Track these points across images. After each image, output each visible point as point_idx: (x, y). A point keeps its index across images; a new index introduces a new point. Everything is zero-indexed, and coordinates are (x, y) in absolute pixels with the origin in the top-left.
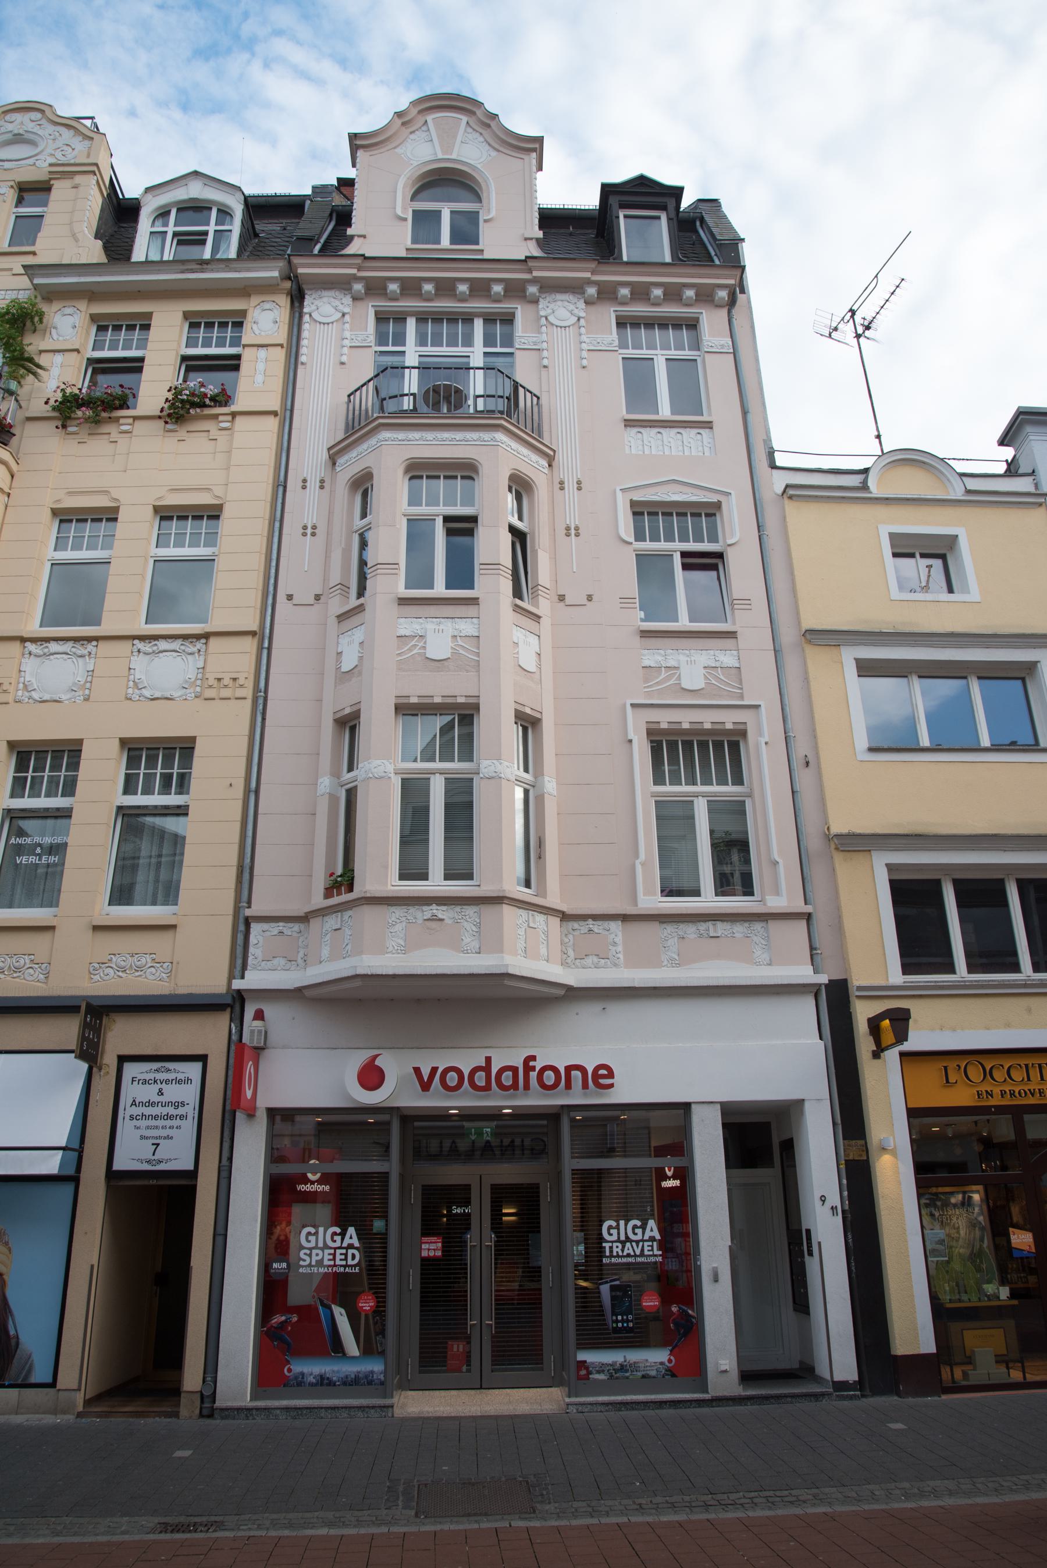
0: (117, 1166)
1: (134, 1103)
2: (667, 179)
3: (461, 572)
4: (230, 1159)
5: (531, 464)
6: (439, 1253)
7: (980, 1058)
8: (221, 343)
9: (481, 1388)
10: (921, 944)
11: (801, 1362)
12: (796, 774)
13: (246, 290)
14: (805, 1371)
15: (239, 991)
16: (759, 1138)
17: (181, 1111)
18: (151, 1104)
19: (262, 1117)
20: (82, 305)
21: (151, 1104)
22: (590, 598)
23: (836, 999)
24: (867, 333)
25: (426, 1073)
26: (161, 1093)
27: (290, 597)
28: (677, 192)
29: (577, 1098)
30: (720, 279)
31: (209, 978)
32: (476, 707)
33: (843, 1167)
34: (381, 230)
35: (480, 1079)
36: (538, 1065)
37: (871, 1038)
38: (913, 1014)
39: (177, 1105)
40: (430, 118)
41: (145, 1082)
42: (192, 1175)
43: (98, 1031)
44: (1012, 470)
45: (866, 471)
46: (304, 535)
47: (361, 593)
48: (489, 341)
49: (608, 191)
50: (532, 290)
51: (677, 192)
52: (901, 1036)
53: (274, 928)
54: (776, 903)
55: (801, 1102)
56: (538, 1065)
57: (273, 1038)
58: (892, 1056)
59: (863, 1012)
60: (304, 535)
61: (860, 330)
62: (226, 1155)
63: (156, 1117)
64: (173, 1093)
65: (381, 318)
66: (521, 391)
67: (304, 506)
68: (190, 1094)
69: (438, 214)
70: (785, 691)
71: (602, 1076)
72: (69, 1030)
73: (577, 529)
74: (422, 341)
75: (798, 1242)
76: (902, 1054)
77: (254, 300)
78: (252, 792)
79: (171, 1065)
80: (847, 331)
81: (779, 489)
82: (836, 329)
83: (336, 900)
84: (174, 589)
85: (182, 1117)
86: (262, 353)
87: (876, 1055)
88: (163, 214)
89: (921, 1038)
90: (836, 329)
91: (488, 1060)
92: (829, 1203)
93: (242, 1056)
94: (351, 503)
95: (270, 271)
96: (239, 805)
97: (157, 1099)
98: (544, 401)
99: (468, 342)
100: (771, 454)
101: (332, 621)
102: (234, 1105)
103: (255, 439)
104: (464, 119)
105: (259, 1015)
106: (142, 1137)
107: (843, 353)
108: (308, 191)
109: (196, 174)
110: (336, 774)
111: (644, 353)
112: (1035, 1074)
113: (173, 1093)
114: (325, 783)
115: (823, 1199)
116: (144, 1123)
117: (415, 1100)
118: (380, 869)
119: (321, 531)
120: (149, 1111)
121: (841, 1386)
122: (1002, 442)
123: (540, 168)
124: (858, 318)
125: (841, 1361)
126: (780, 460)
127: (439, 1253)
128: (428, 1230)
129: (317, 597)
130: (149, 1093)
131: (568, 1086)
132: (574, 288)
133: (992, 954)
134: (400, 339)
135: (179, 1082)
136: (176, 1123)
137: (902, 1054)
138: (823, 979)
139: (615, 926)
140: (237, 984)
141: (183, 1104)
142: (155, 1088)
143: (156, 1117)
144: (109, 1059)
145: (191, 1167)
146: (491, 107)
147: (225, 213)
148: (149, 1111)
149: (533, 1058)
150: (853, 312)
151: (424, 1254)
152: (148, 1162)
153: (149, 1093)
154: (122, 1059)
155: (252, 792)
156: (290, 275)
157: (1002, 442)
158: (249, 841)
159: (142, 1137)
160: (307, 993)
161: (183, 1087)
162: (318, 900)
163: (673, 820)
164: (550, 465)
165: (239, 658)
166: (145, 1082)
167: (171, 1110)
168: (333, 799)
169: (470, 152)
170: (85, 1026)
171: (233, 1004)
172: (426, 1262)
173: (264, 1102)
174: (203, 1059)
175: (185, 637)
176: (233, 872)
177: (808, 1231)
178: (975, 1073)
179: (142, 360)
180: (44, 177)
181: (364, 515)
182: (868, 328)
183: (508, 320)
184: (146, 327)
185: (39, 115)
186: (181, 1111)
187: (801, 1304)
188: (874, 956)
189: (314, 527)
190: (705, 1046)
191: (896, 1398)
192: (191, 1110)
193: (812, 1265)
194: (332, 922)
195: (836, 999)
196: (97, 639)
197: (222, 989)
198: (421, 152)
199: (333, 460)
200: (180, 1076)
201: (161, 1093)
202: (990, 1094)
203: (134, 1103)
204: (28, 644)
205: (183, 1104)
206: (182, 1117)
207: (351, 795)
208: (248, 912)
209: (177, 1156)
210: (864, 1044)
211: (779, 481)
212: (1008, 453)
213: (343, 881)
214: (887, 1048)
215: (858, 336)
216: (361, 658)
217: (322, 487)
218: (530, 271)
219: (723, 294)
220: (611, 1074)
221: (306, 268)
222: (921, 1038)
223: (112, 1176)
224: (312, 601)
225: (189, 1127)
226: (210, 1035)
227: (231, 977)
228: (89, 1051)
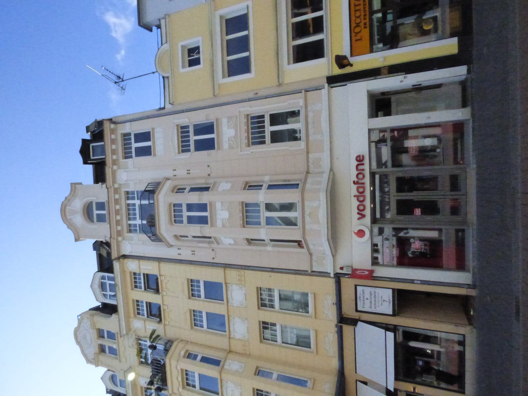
0: (391, 313)
1: (371, 307)
2: (79, 145)
3: (203, 207)
4: (389, 278)
5: (167, 186)
6: (420, 209)
7: (352, 28)
8: (140, 279)
9: (466, 195)
10: (313, 52)
11: (459, 84)
12: (353, 44)
13: (123, 272)
14: (463, 84)
15: (334, 275)
16: (381, 105)
17: (373, 293)
18: (371, 302)
19: (375, 268)
20: (131, 320)
21: (371, 302)
22: (208, 166)
23: (332, 80)
24: (122, 78)
25: (359, 216)
26: (367, 299)
27: (213, 258)
28: (84, 141)
29: (366, 167)
30: (107, 127)
31: (331, 283)
32: (243, 202)
33: (390, 75)
34: (102, 231)
35: (361, 199)
36: (356, 180)
37: (346, 68)
38: (337, 54)
39: (371, 294)
40: (68, 217)
41: (364, 304)
42: (394, 290)
43: (348, 319)
44: (159, 27)
45: (163, 77)
46: (194, 254)
47: (210, 238)
48: (133, 198)
49: (85, 162)
50: (116, 186)
51: (84, 141)
52: (345, 57)
53: (314, 264)
54: (301, 102)
55: (368, 91)
56: (356, 180)
57: (349, 264)
58: (352, 60)
59: (337, 71)
60: (194, 254)
61: (121, 80)
62: (387, 279)
63: (375, 301)
64: (367, 296)
65: (130, 231)
66: (147, 189)
67: (186, 254)
68: (367, 290)
69: (98, 215)
70: (239, 98)
71: (360, 160)
72: (347, 329)
73: (187, 171)
74: (135, 219)
75: (418, 89)
76: (352, 55)
77: (126, 269)
78: (273, 270)
79: (358, 296)
80: (122, 84)
81: (170, 106)
82: (122, 88)
83: (305, 246)
84: (214, 291)
85: (375, 293)
86: (141, 267)
87: (351, 65)
88: (105, 295)
89: (346, 51)
90: (122, 88)
91: (355, 196)
92: (403, 80)
93: (355, 274)
94: (184, 240)
95: (116, 265)
96: (276, 274)
97: (369, 301)
98: (150, 182)
99: (134, 205)
100: (161, 109)
101: (220, 246)
102: (370, 276)
103: (167, 269)
104: (68, 207)
105: (342, 268)
106: (382, 305)
107: (128, 84)
108: (95, 252)
109: (91, 286)
110: (266, 245)
111: (133, 150)
112: (357, 8)
113: (367, 296)
114: (269, 248)
115: (402, 81)
116: (377, 305)
117: (368, 219)
118: (293, 233)
119: (193, 249)
120: (373, 302)
121: (469, 71)
122: (151, 30)
123: (81, 184)
124: (117, 81)
125: (461, 71)
126: (162, 106)
127: (420, 209)
128: (411, 213)
129: (213, 250)
130: (367, 302)
131: (363, 170)
132: (114, 173)
133: (318, 25)
134: (135, 225)
135: (363, 293)
136: (377, 295)
137: (352, 55)
138: (326, 85)
139: (311, 156)
140: (332, 275)
141: (371, 292)
142: (366, 301)
143: (375, 301)
144: (356, 315)
145: (391, 290)
146: (63, 199)
147: (103, 278)
148: (373, 302)
149: (354, 182)
150: (116, 83)
151: (420, 214)
152: (389, 303)
153: (367, 302)
154: (357, 310)
155: (273, 270)
156: (118, 258)
157: (151, 30)
158: (287, 271)
159: (382, 305)
160: (334, 253)
161: (365, 292)
162: (304, 250)
163: (276, 137)
164: (169, 179)
165: (232, 274)
166: (364, 304)
167: (373, 296)
168: (274, 246)
169: (78, 204)
170: (346, 323)
171: (338, 277)
172: (423, 213)
173: (370, 267)
174: (356, 286)
175: (227, 290)
176: (297, 276)
177: (413, 86)
178: (357, 30)
179: (146, 303)
180: (95, 331)
181: (187, 237)
182: (120, 78)
183: (127, 193)
184: (137, 301)
185: (78, 332)
186: (373, 293)
187: (439, 86)
188: (320, 68)
189: (192, 251)
190: (345, 127)
191: (473, 52)
192: (373, 290)
193: (424, 84)
194: (311, 247)
195: (332, 80)
196: (228, 316)
197: (334, 280)
198: (79, 220)
199: (172, 246)
200: (362, 293)
201: (367, 299)
202: (365, 24)
203: (371, 307)
204: (231, 336)
205: (371, 292)
206: (375, 293)
207: (272, 240)
208: (310, 272)
209: (388, 295)
210: (347, 70)
211: (168, 106)
212: (154, 28)
213: (299, 243)
214: (349, 62)
215: (123, 81)
216: (230, 238)
217: (180, 249)
218: (111, 187)
219: (112, 126)
220: (359, 156)
221: (114, 255)
222: (346, 51)
223: (394, 315)
224: (214, 252)
225: (378, 290)
226: (348, 284)
227: (330, 277)
228: (354, 322)
